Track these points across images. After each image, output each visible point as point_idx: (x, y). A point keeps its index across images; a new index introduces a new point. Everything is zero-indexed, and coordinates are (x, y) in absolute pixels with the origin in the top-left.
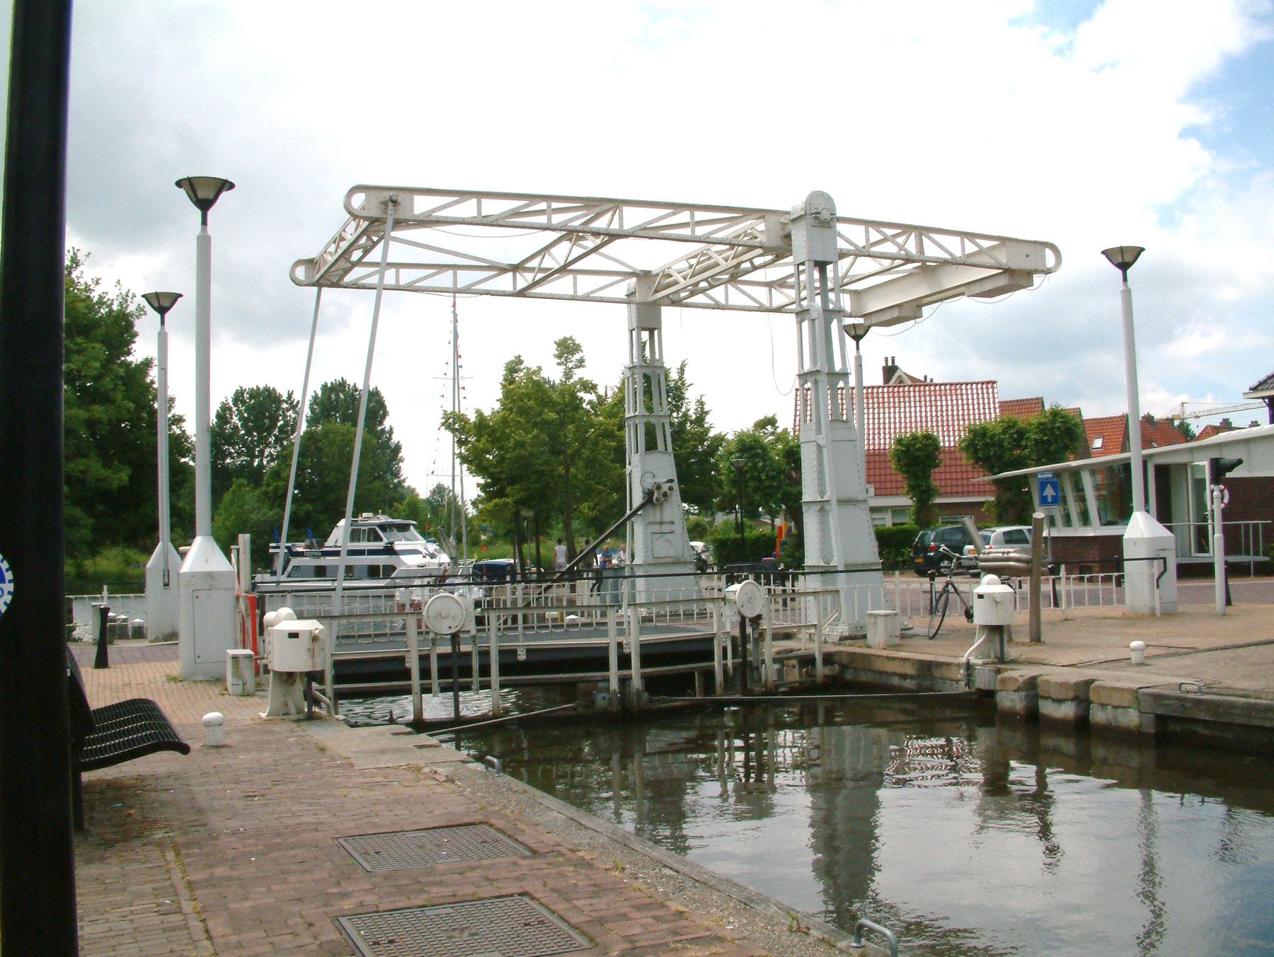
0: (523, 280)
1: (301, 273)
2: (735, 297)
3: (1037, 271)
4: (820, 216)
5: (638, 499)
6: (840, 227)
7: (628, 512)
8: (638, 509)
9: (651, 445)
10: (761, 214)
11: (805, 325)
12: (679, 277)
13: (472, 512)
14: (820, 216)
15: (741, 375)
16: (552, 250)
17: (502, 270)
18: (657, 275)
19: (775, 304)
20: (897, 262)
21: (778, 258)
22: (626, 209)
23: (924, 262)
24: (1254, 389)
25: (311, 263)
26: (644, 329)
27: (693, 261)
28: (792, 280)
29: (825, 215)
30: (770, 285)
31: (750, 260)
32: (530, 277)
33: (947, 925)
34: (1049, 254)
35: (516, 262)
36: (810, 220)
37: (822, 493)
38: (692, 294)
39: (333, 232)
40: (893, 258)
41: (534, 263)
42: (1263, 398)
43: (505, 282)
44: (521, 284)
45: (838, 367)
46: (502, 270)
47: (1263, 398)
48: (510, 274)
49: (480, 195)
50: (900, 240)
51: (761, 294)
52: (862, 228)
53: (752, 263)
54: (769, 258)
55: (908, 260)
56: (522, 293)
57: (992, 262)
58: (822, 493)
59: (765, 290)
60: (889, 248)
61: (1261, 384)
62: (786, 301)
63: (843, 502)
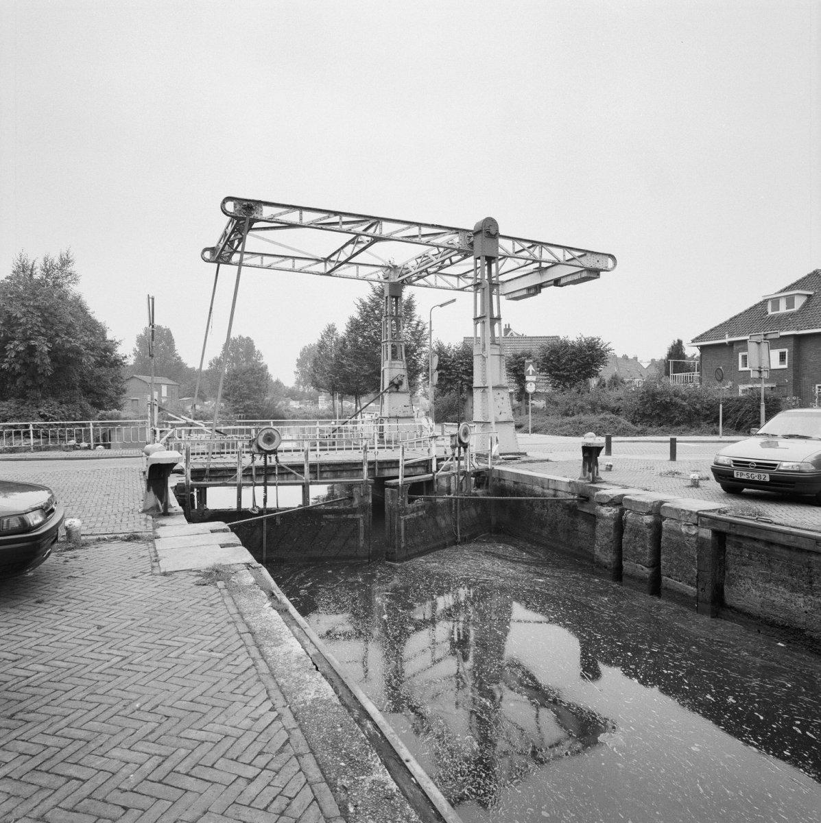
0: (330, 266)
1: (207, 255)
2: (440, 281)
3: (603, 270)
4: (488, 230)
5: (386, 385)
6: (501, 241)
7: (381, 391)
8: (387, 389)
9: (394, 357)
10: (457, 231)
11: (479, 295)
12: (411, 269)
13: (80, 358)
14: (488, 230)
15: (445, 316)
16: (344, 249)
17: (318, 261)
18: (400, 268)
19: (461, 287)
20: (529, 262)
21: (466, 256)
22: (384, 223)
23: (540, 262)
24: (693, 341)
25: (212, 250)
26: (393, 297)
27: (419, 260)
28: (472, 273)
29: (493, 232)
30: (458, 276)
31: (450, 258)
32: (333, 265)
33: (359, 311)
34: (610, 261)
35: (326, 257)
36: (484, 233)
37: (485, 382)
38: (419, 278)
39: (222, 232)
40: (527, 259)
41: (333, 258)
42: (697, 346)
43: (321, 267)
44: (329, 268)
45: (495, 315)
46: (318, 261)
47: (697, 346)
48: (323, 263)
49: (301, 209)
50: (531, 250)
51: (454, 281)
52: (510, 242)
53: (451, 261)
54: (459, 257)
55: (534, 261)
56: (329, 274)
57: (580, 264)
58: (485, 382)
59: (456, 279)
60: (525, 254)
61: (697, 338)
62: (465, 285)
63: (494, 388)
